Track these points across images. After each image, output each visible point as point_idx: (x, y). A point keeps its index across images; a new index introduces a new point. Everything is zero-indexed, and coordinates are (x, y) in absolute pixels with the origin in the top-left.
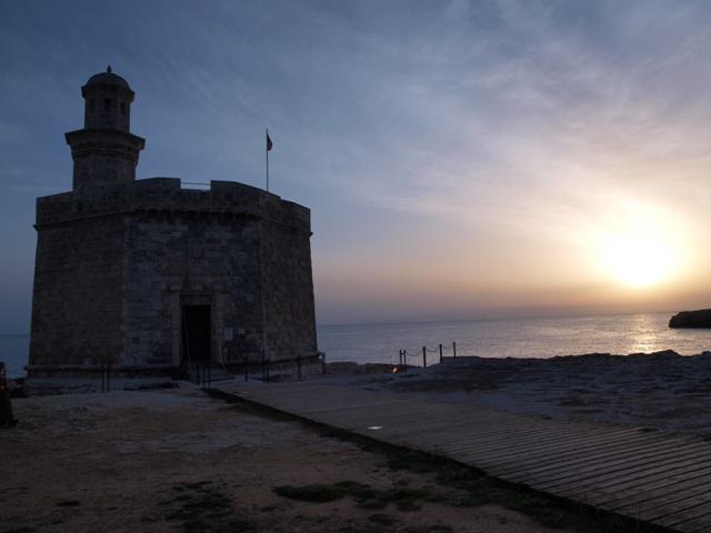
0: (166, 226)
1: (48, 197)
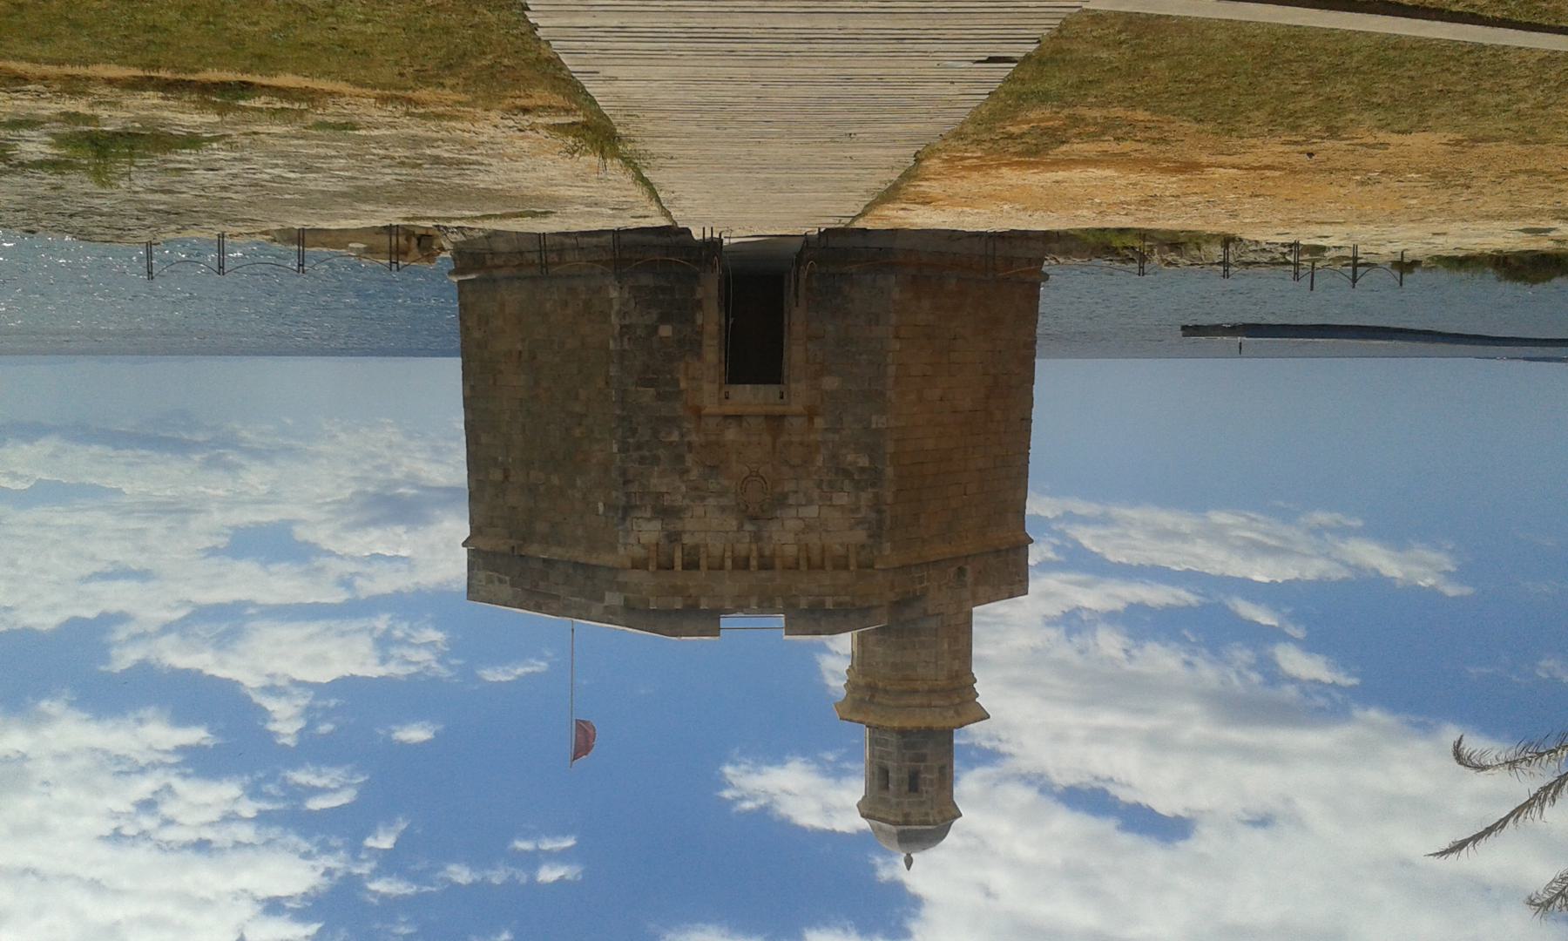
0: (813, 540)
1: (1011, 596)
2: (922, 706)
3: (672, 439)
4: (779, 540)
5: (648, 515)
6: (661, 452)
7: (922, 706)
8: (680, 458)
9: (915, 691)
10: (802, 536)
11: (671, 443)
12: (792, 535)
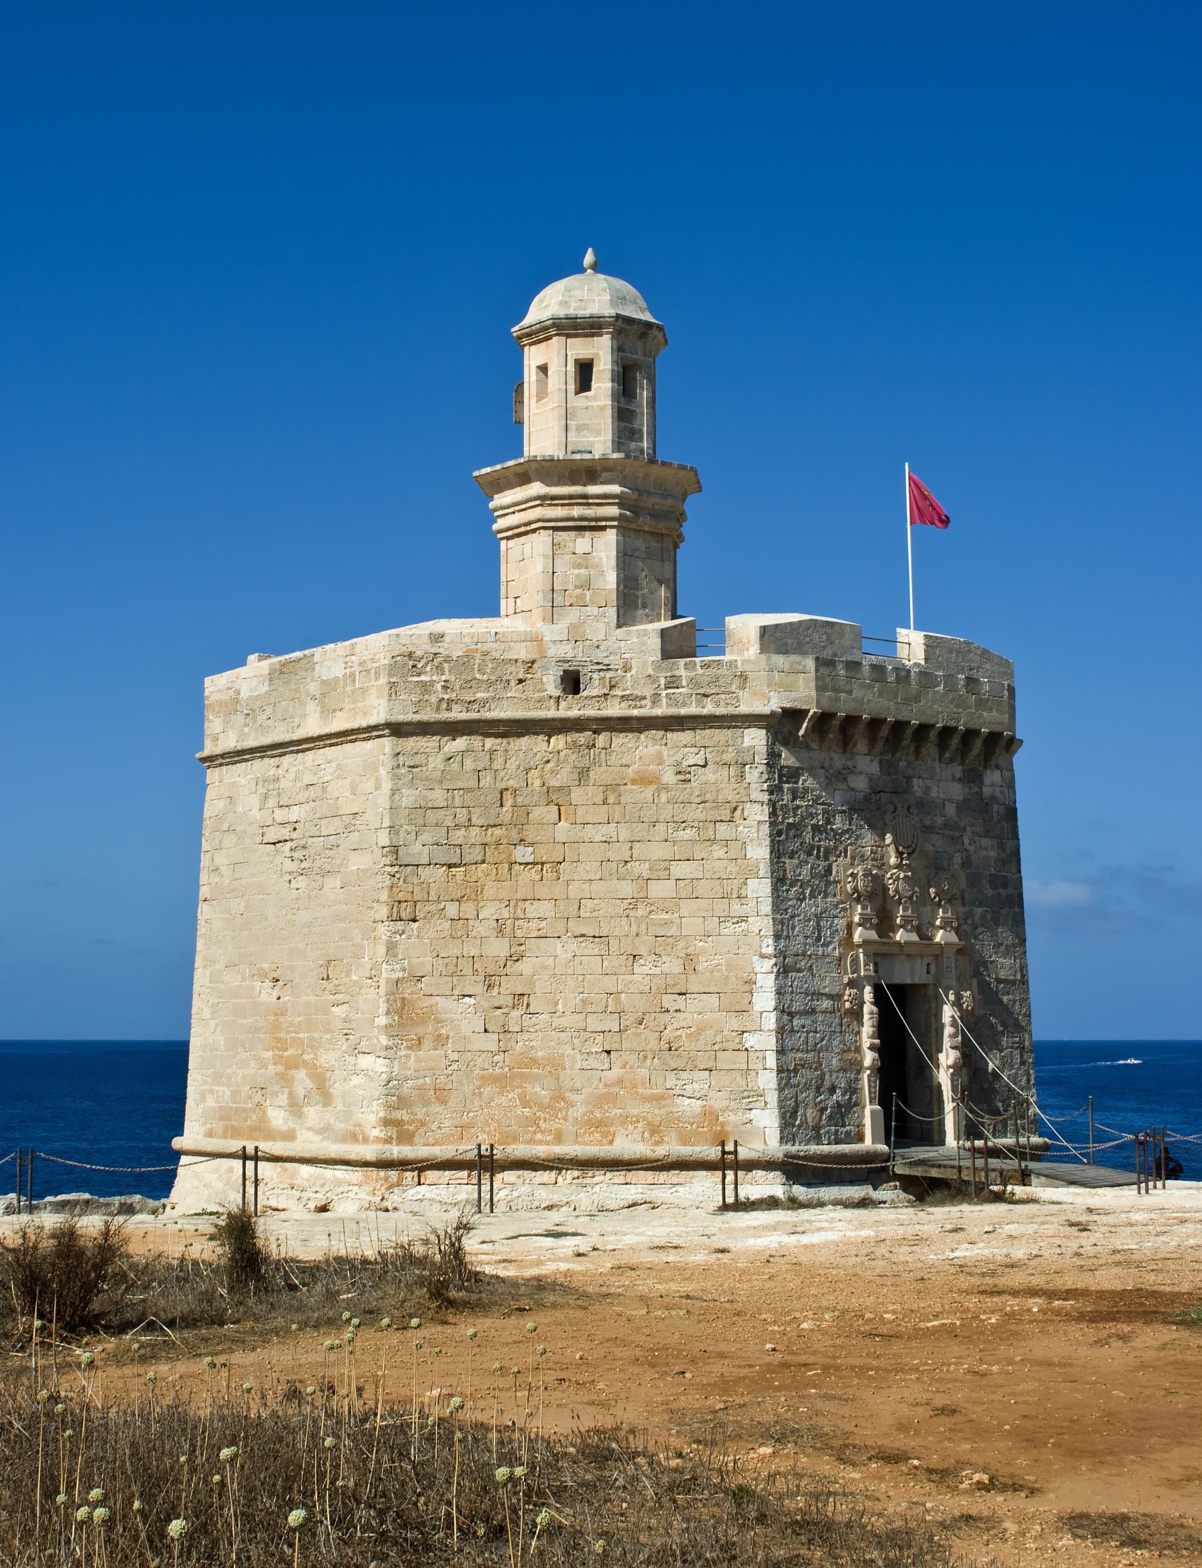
0: (839, 761)
2: (649, 493)
3: (980, 910)
4: (872, 761)
5: (995, 807)
6: (989, 892)
7: (649, 493)
8: (973, 882)
9: (655, 515)
10: (850, 764)
11: (981, 905)
12: (859, 768)
